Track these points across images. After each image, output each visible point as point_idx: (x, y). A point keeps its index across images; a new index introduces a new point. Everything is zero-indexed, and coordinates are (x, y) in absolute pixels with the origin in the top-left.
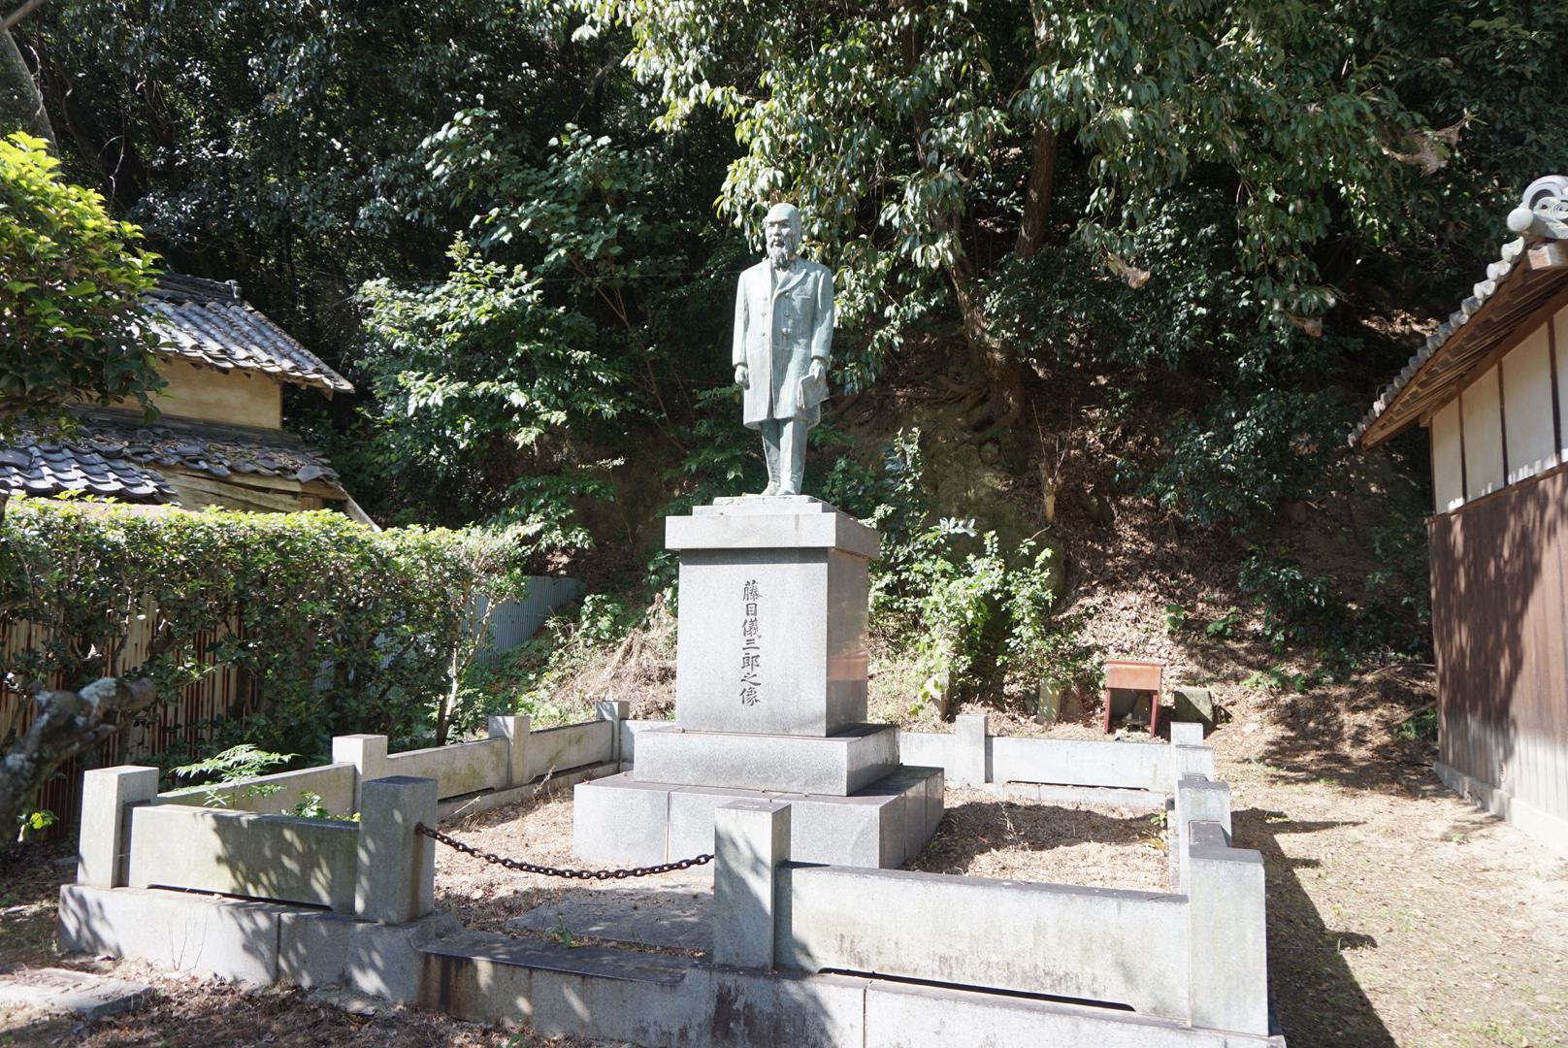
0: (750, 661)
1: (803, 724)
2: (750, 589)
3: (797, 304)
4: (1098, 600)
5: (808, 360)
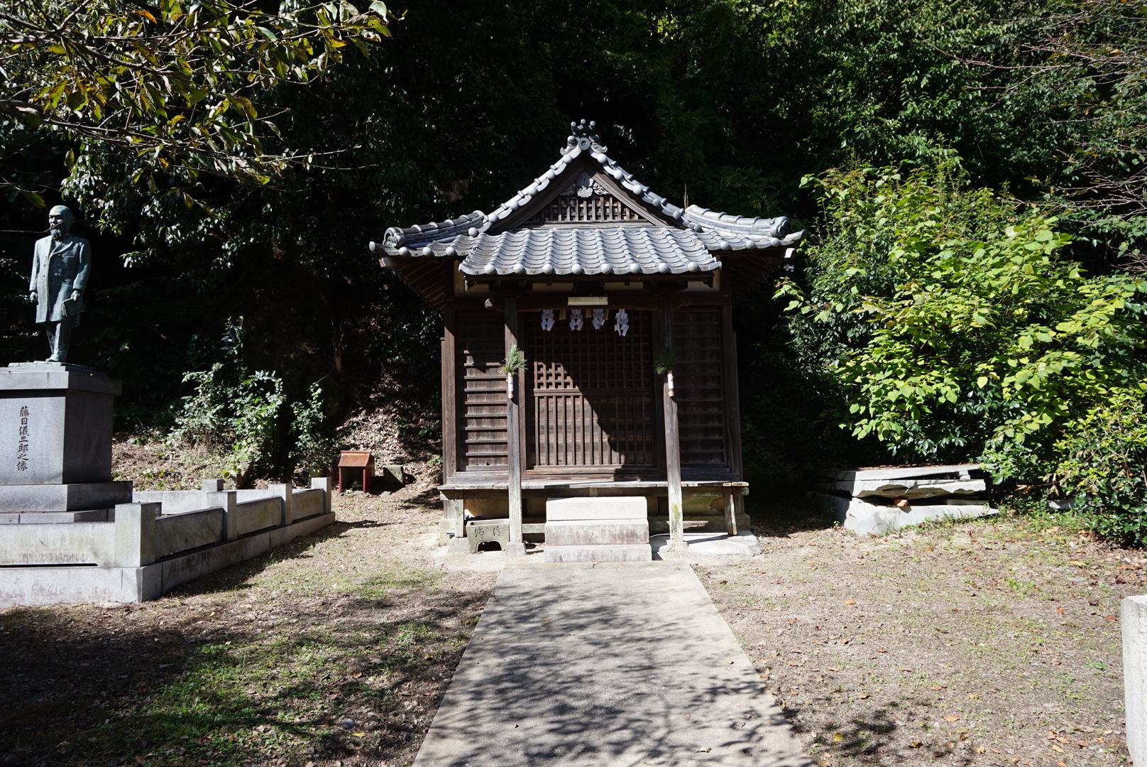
0: (23, 448)
1: (50, 478)
2: (24, 411)
3: (65, 260)
4: (360, 418)
5: (70, 291)
